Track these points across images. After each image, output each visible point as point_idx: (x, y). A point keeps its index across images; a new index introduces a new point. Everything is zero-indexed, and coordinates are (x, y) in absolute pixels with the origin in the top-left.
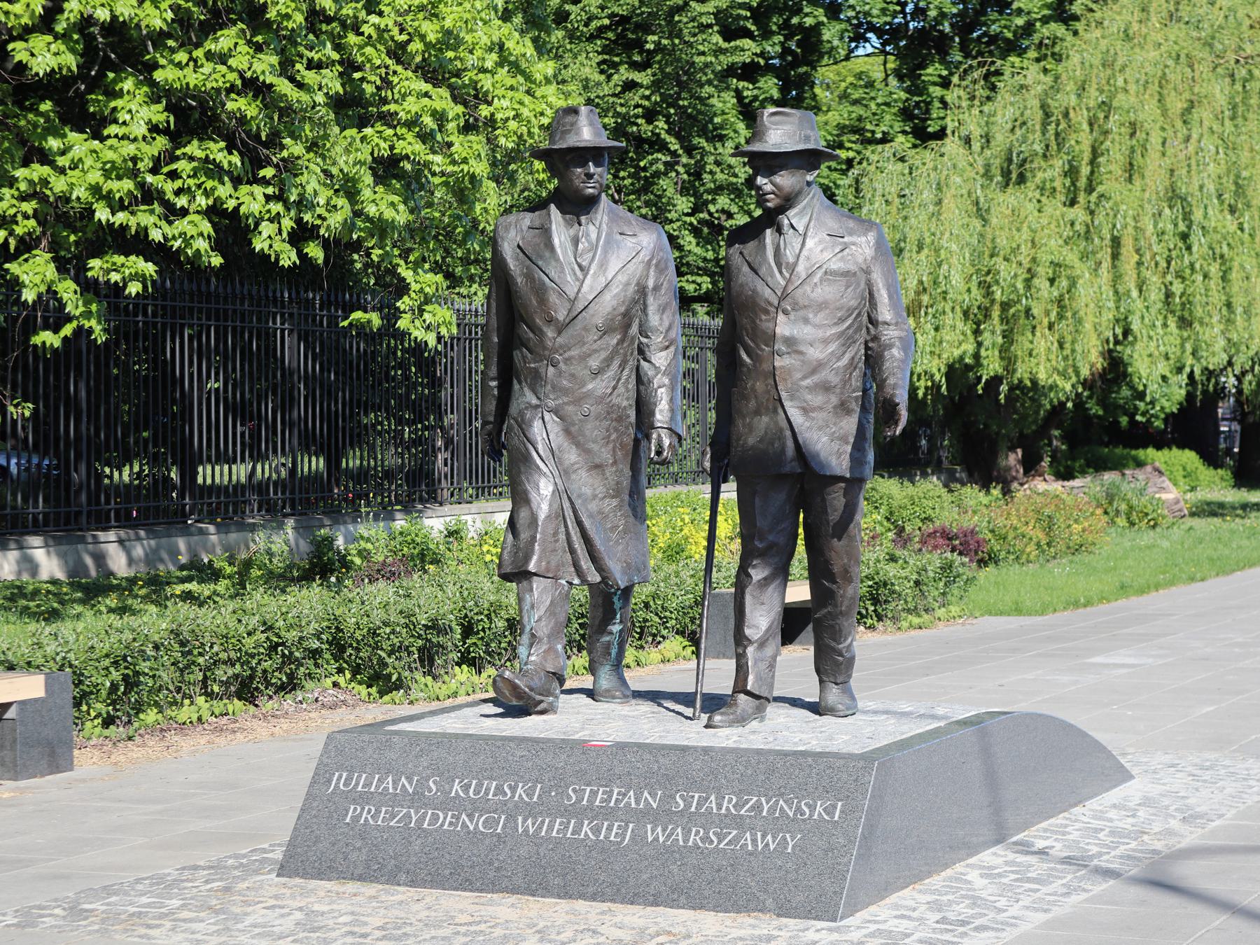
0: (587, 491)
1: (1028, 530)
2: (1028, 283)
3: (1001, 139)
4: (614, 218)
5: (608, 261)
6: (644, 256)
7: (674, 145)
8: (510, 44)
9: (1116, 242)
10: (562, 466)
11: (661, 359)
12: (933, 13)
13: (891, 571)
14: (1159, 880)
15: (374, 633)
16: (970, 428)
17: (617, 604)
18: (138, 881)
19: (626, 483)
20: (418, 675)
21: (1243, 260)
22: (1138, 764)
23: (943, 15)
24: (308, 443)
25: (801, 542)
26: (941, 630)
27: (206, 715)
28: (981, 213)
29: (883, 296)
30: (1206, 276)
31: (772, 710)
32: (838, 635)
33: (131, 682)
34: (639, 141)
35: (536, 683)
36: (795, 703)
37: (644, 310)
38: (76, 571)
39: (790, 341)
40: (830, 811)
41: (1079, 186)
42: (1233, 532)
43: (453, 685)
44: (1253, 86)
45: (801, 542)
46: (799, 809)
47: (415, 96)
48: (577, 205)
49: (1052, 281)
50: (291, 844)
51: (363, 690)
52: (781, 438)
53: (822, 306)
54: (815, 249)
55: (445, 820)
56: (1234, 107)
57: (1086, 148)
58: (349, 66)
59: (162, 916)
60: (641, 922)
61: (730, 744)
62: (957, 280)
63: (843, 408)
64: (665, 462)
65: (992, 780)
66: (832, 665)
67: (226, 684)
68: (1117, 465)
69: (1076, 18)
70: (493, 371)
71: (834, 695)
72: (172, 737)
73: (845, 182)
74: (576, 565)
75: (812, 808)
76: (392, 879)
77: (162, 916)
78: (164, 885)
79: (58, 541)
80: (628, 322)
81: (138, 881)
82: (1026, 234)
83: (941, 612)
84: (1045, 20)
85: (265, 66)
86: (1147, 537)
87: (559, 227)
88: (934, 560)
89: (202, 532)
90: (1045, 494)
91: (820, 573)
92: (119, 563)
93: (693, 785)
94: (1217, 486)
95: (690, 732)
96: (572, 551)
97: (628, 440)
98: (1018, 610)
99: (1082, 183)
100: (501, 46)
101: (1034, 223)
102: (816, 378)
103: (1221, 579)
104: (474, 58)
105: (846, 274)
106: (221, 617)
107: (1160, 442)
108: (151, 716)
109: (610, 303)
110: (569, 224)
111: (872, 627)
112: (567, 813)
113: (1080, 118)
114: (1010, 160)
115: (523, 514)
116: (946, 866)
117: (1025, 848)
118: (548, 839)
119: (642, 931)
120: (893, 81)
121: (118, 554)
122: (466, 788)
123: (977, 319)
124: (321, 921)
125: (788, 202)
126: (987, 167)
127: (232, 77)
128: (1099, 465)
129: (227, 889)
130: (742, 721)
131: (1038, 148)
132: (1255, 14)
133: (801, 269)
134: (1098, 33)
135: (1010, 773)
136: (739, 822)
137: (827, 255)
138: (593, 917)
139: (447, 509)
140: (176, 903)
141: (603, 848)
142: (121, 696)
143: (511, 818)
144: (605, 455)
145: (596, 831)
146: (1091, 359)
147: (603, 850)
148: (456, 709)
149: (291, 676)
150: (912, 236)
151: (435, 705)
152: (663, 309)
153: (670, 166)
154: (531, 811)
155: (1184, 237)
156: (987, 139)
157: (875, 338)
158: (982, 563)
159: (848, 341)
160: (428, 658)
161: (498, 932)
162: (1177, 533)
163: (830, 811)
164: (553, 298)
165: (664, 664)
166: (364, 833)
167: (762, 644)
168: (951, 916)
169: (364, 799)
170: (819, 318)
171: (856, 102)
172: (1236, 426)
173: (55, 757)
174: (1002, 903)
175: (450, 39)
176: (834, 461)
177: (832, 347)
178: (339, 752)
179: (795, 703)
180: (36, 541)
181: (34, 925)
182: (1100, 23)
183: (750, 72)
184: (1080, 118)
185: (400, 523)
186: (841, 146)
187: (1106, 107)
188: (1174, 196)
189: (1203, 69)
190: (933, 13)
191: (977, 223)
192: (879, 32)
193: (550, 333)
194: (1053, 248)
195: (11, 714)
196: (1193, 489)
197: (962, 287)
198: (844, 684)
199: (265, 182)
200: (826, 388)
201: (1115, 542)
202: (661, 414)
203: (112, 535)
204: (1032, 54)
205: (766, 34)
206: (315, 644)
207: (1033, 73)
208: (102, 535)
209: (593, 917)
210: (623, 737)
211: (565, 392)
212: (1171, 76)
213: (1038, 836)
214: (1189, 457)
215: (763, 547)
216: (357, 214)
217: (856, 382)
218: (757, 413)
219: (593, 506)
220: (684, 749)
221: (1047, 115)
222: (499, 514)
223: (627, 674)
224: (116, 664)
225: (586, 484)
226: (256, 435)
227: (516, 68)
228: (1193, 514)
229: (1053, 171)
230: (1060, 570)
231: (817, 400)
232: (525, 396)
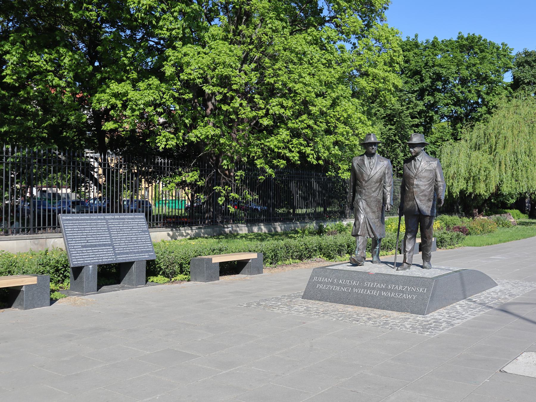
0: (371, 217)
1: (478, 227)
2: (479, 172)
3: (474, 140)
4: (378, 158)
5: (377, 167)
6: (385, 166)
7: (400, 142)
8: (362, 118)
9: (500, 162)
10: (366, 212)
11: (388, 189)
12: (459, 113)
13: (445, 236)
14: (503, 310)
15: (328, 246)
16: (464, 204)
17: (378, 242)
18: (273, 298)
19: (380, 216)
20: (337, 256)
21: (531, 167)
22: (499, 282)
23: (461, 113)
24: (318, 205)
25: (419, 231)
26: (456, 249)
27: (291, 263)
28: (469, 157)
29: (439, 175)
30: (522, 171)
31: (411, 267)
32: (427, 251)
33: (276, 255)
34: (392, 141)
35: (359, 259)
36: (418, 265)
37: (385, 178)
38: (270, 231)
39: (417, 185)
40: (423, 290)
41: (492, 150)
42: (527, 229)
43: (345, 258)
44: (535, 128)
45: (419, 231)
46: (416, 290)
47: (341, 129)
48: (370, 155)
49: (485, 171)
50: (305, 292)
51: (326, 258)
52: (415, 207)
53: (424, 177)
54: (424, 164)
55: (338, 288)
56: (530, 133)
57: (494, 142)
58: (327, 123)
59: (276, 306)
60: (380, 313)
61: (401, 274)
62: (463, 171)
63: (429, 200)
64: (389, 211)
65: (463, 284)
66: (426, 257)
67: (296, 256)
68: (500, 213)
69: (492, 113)
70: (352, 191)
71: (426, 264)
72: (284, 267)
73: (438, 150)
74: (369, 233)
75: (419, 289)
76: (326, 301)
77: (276, 306)
78: (278, 300)
79: (266, 225)
80: (381, 180)
81: (273, 298)
82: (479, 161)
83: (456, 245)
84: (485, 114)
85: (311, 122)
86: (507, 229)
87: (366, 160)
88: (455, 234)
89: (297, 223)
90: (483, 219)
91: (423, 237)
92: (279, 230)
93: (393, 283)
94: (524, 218)
95: (393, 271)
96: (368, 230)
97: (381, 206)
98: (475, 246)
99: (493, 150)
100: (360, 118)
101: (481, 158)
102: (423, 193)
103: (524, 239)
104: (354, 121)
105: (430, 170)
106: (296, 242)
107: (511, 208)
108: (280, 263)
109: (377, 176)
110: (368, 159)
111: (440, 248)
112: (365, 288)
113: (493, 136)
114: (476, 145)
115: (357, 222)
116: (451, 304)
117: (470, 300)
118: (360, 293)
119: (380, 315)
120: (450, 127)
121: (279, 227)
122: (343, 282)
123: (467, 180)
124: (310, 309)
125: (417, 154)
126: (471, 147)
127: (305, 125)
128: (496, 213)
129: (291, 301)
130: (405, 269)
131: (483, 142)
132: (535, 111)
133: (420, 169)
134: (497, 116)
135: (467, 283)
136: (403, 292)
137: (426, 166)
138: (369, 311)
139: (348, 220)
140: (280, 303)
141: (372, 296)
142: (273, 258)
143: (352, 289)
144: (376, 210)
145: (371, 292)
146: (493, 189)
147: (372, 297)
148: (342, 263)
149: (310, 255)
150: (453, 161)
151: (341, 262)
152: (389, 178)
153: (399, 146)
154: (357, 287)
155: (517, 161)
156: (471, 140)
157: (437, 185)
158: (467, 234)
159: (430, 185)
160: (340, 252)
161: (348, 314)
162: (514, 229)
163: (423, 290)
164: (365, 175)
165: (390, 256)
166: (320, 290)
167: (410, 252)
168: (451, 315)
169: (321, 283)
170: (424, 180)
171: (441, 132)
172: (530, 205)
173: (259, 271)
174: (464, 313)
175: (349, 116)
176: (427, 212)
177: (427, 187)
178: (316, 272)
179: (418, 265)
180: (262, 224)
181: (250, 307)
182: (497, 114)
183: (417, 126)
184: (493, 136)
185: (338, 223)
186: (437, 142)
187: (499, 133)
188: (515, 153)
189: (522, 124)
190: (459, 113)
191: (468, 159)
192: (447, 116)
193: (364, 183)
194: (485, 164)
195: (250, 261)
196: (519, 219)
197: (464, 173)
198: (429, 262)
199: (310, 146)
200: (425, 196)
201: (499, 231)
202: (388, 200)
203: (277, 224)
204: (482, 121)
205: (421, 118)
206: (316, 248)
207: (482, 125)
208: (275, 224)
209: (369, 311)
210: (377, 272)
211: (367, 196)
212: (515, 126)
213: (474, 298)
214: (517, 211)
215: (411, 231)
216: (330, 153)
217: (432, 194)
218: (409, 201)
219: (373, 221)
220: (391, 275)
221: (485, 135)
222: (352, 221)
223: (380, 258)
224: (273, 251)
225: (371, 216)
226: (307, 203)
227: (363, 123)
228: (518, 224)
229: (486, 147)
230: (485, 237)
231: (423, 198)
232: (358, 196)
